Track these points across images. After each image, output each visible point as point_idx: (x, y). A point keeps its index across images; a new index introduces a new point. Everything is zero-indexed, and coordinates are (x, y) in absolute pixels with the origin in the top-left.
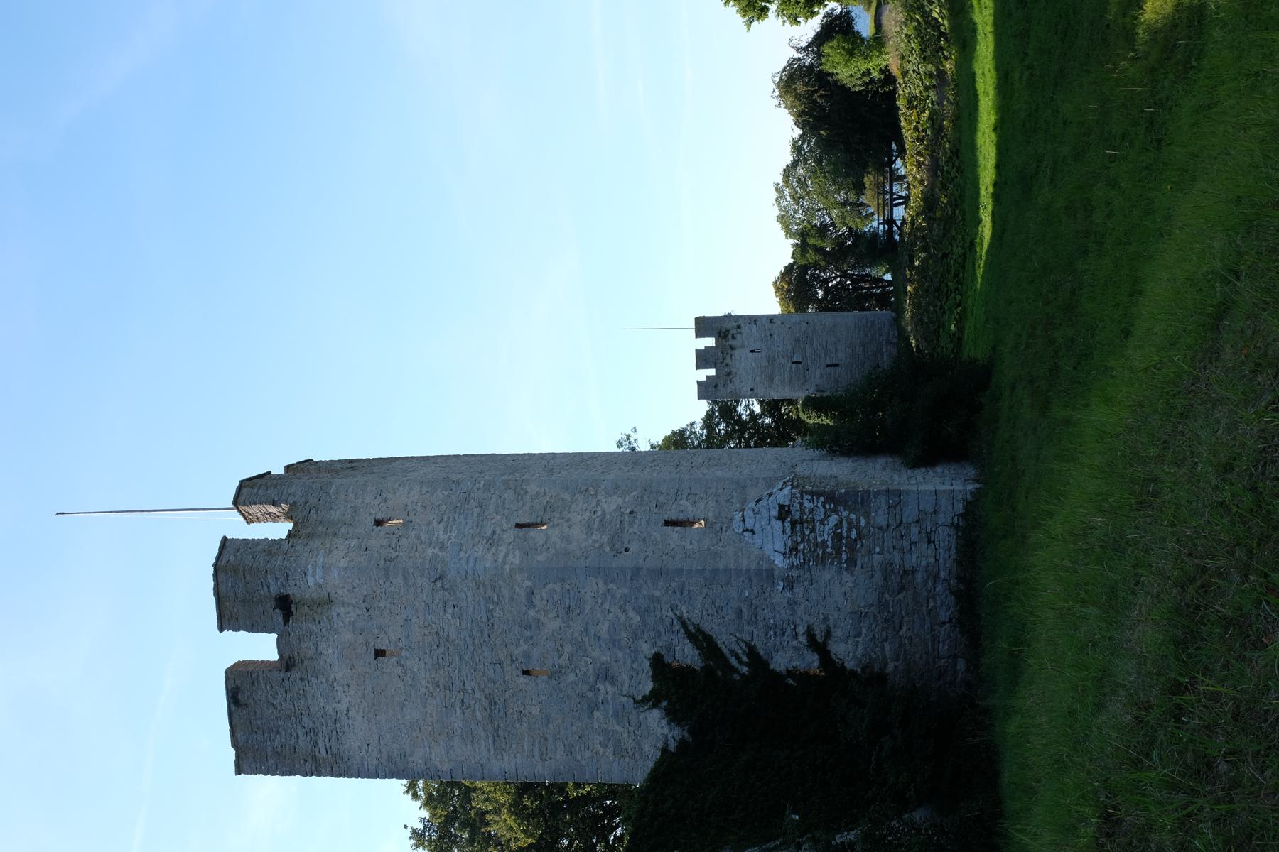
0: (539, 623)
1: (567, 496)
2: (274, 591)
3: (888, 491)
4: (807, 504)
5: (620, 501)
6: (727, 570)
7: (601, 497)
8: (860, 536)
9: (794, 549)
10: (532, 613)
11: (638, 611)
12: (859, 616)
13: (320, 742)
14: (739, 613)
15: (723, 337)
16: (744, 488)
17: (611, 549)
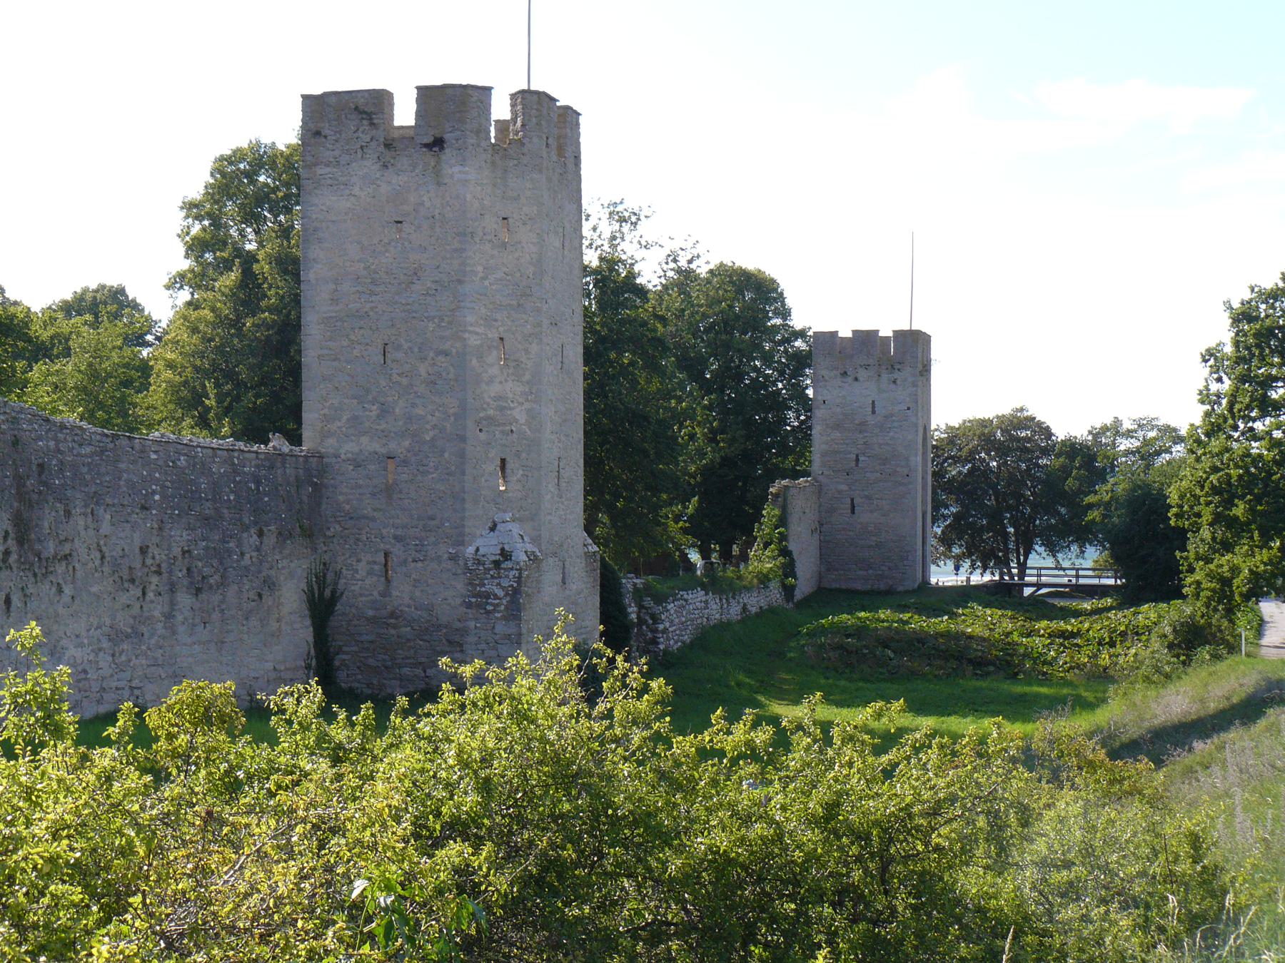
0: (423, 359)
1: (527, 377)
2: (447, 136)
3: (520, 635)
4: (512, 573)
5: (523, 421)
6: (464, 510)
7: (527, 405)
8: (488, 612)
9: (479, 562)
10: (432, 354)
11: (433, 439)
12: (430, 608)
13: (329, 169)
14: (432, 518)
15: (906, 356)
16: (532, 520)
17: (482, 418)
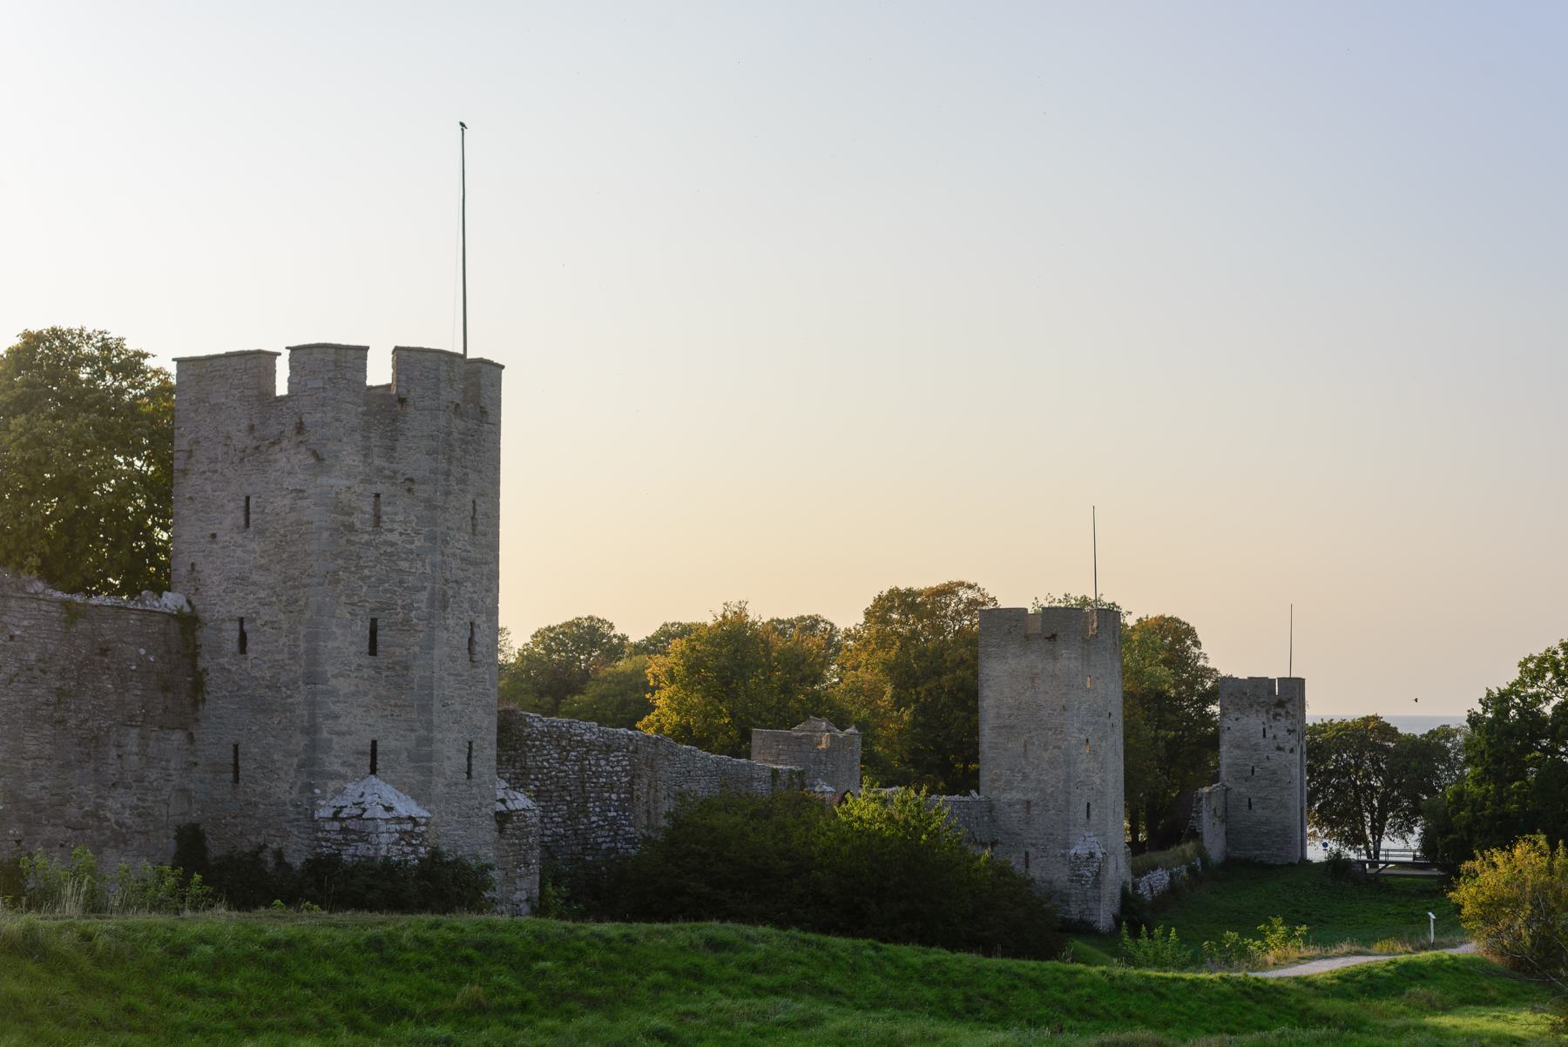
12: (1051, 882)
